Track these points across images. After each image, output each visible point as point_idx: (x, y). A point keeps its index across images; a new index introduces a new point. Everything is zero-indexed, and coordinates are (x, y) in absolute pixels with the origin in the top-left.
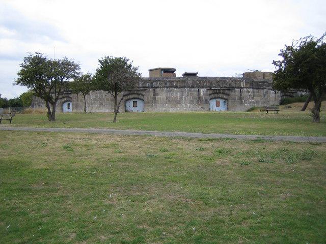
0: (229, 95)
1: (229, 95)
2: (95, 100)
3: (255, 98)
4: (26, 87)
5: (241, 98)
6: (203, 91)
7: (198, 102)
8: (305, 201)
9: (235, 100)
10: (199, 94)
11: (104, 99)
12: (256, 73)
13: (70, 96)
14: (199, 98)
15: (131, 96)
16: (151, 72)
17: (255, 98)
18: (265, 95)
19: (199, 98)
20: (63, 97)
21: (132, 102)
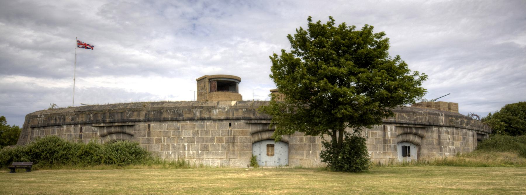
0: (422, 137)
1: (422, 137)
2: (191, 141)
3: (455, 142)
4: (308, 28)
5: (440, 143)
6: (391, 130)
7: (384, 149)
8: (46, 136)
9: (433, 145)
10: (385, 135)
11: (212, 140)
12: (509, 105)
13: (127, 130)
14: (385, 141)
15: (266, 136)
16: (199, 82)
17: (455, 142)
18: (464, 139)
19: (385, 141)
20: (110, 134)
21: (264, 146)
